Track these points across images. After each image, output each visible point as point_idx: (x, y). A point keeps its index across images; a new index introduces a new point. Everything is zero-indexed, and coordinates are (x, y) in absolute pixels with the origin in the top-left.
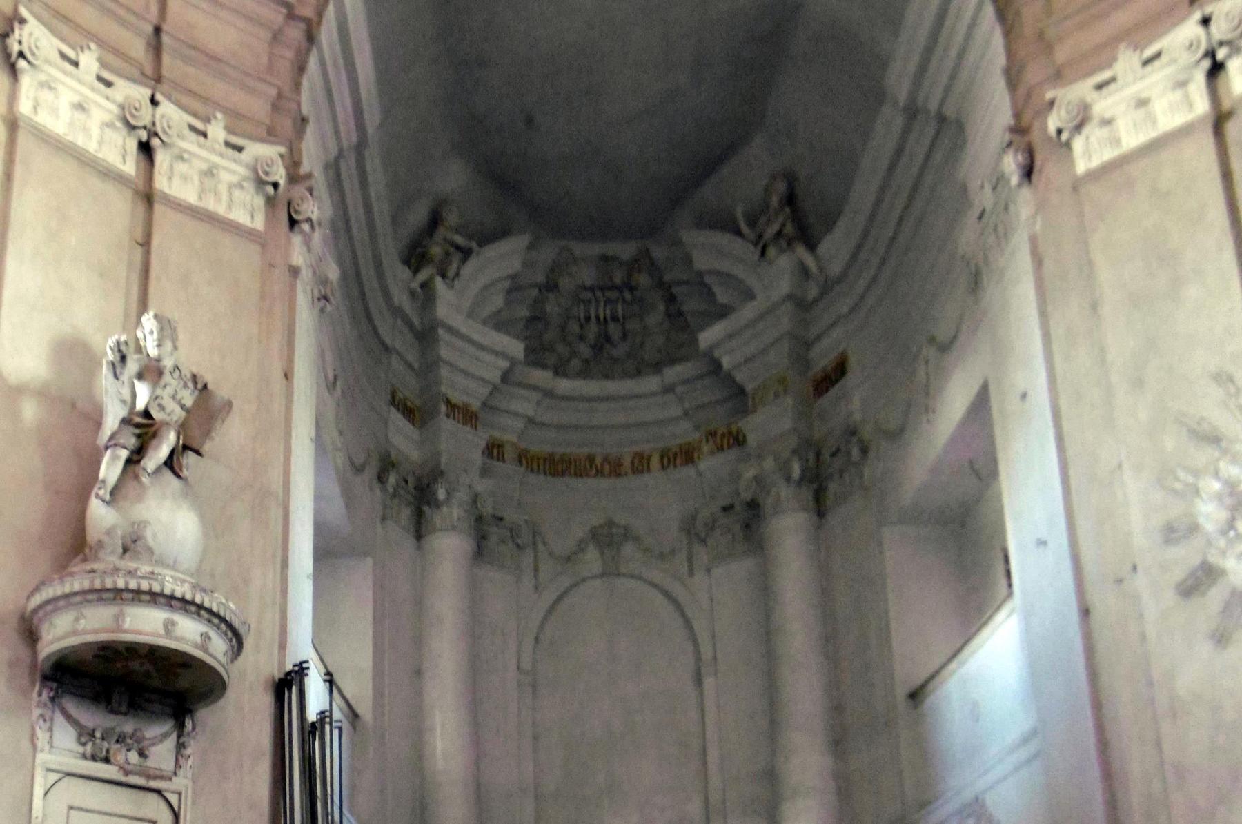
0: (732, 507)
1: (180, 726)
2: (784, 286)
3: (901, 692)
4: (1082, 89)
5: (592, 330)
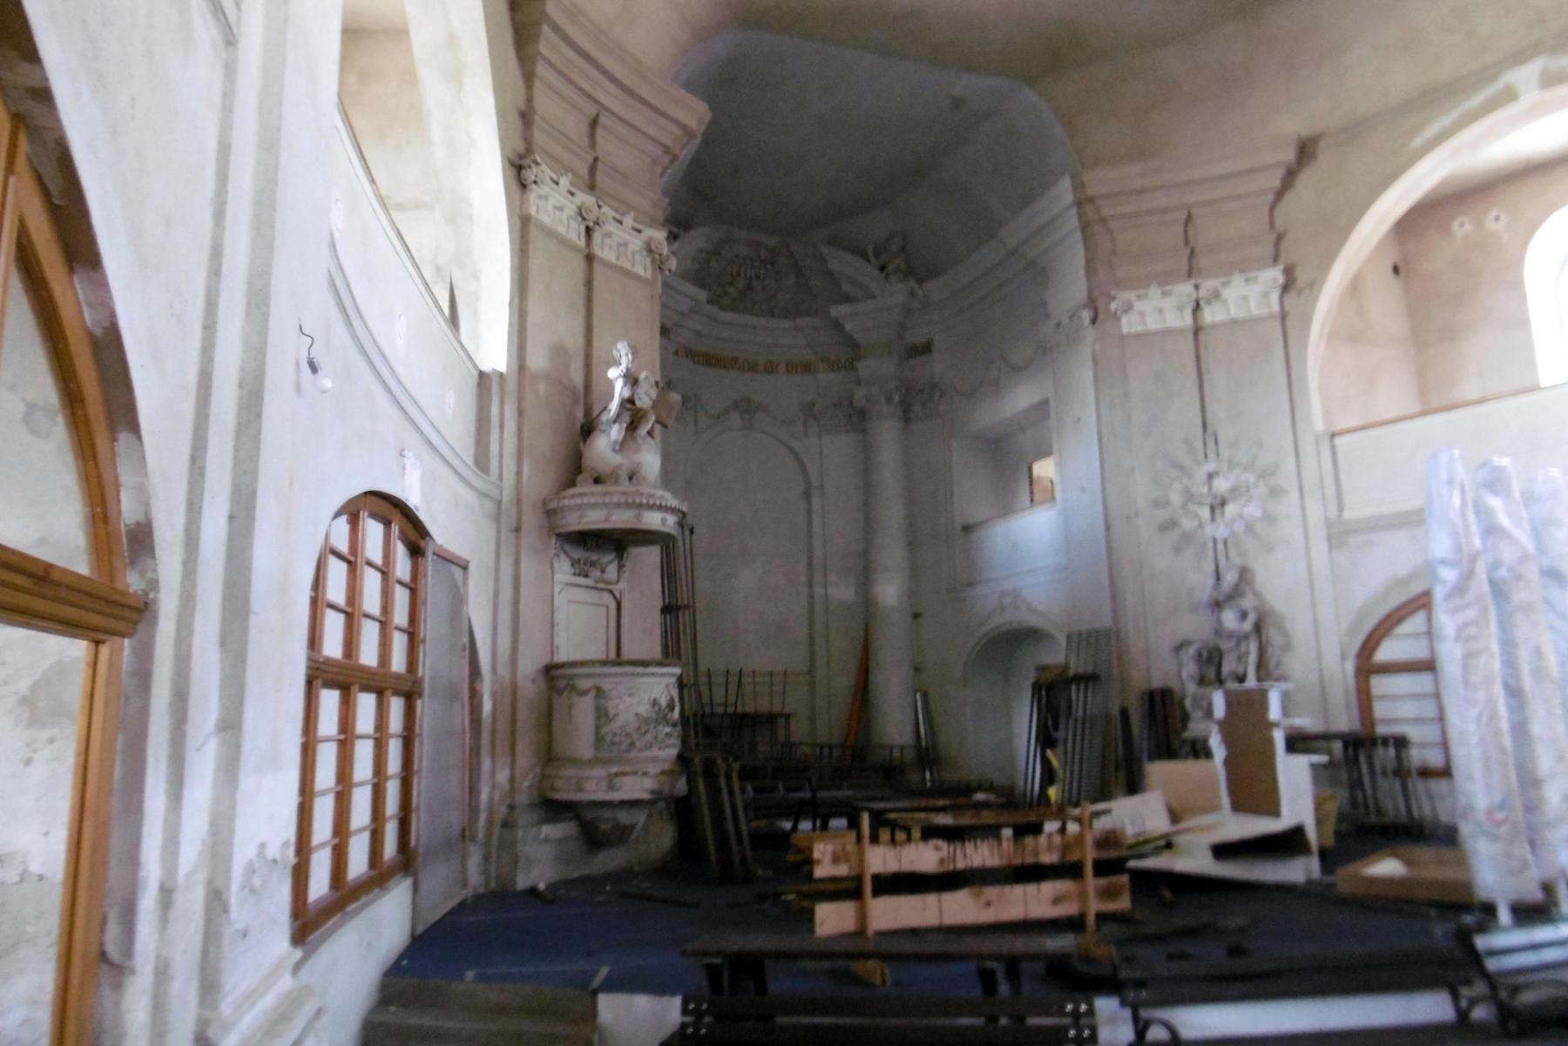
1: (620, 557)
3: (958, 526)
4: (1129, 295)
5: (741, 284)
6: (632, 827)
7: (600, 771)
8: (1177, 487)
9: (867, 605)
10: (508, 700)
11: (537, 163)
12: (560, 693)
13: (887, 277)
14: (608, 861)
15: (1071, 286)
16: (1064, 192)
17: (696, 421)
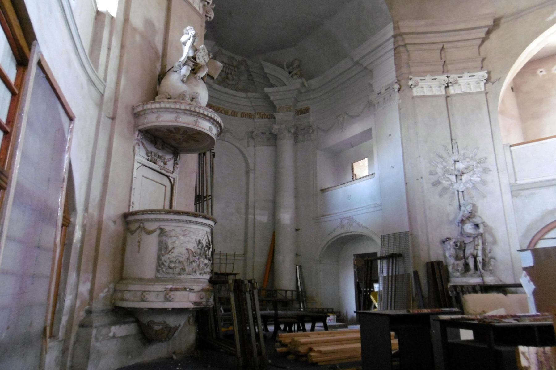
0: (265, 133)
2: (298, 86)
3: (319, 189)
4: (418, 79)
6: (176, 328)
7: (159, 287)
8: (440, 166)
10: (94, 232)
12: (133, 232)
13: (292, 76)
14: (155, 352)
15: (387, 72)
16: (389, 31)
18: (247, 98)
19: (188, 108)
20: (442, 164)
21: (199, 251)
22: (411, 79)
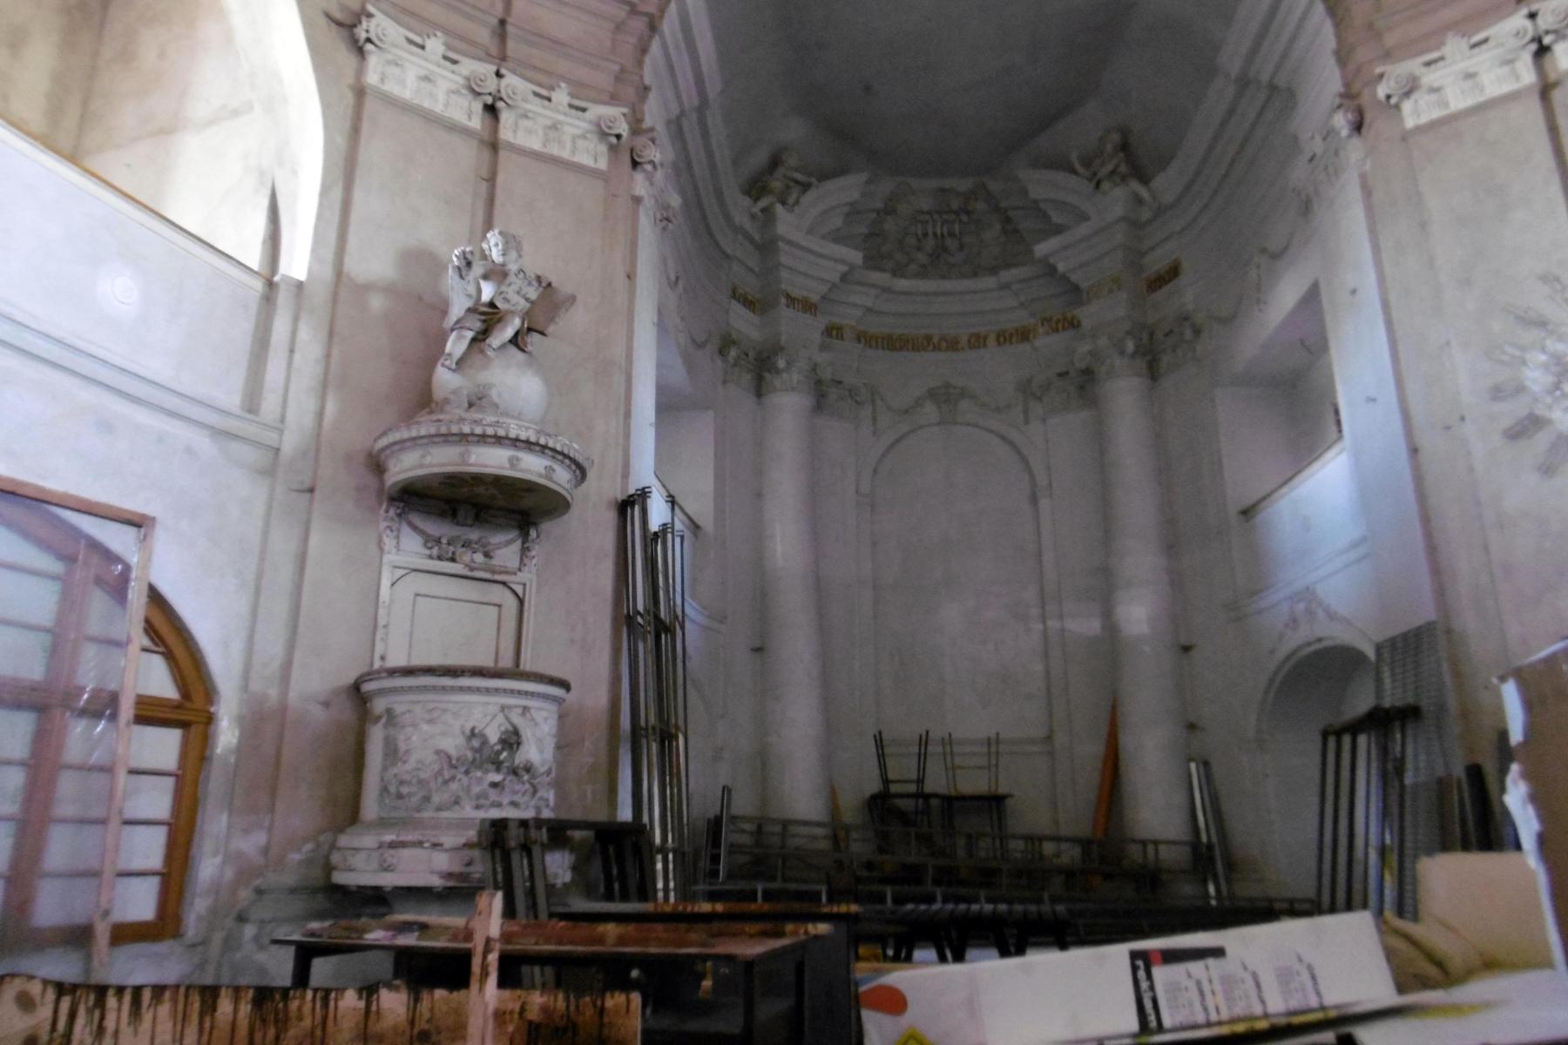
1: (525, 536)
2: (1118, 210)
3: (1233, 510)
4: (1413, 65)
5: (930, 243)
9: (1111, 641)
11: (370, 16)
17: (874, 419)
18: (1005, 287)
19: (433, 431)
20: (1543, 350)
21: (470, 755)
22: (1381, 76)
